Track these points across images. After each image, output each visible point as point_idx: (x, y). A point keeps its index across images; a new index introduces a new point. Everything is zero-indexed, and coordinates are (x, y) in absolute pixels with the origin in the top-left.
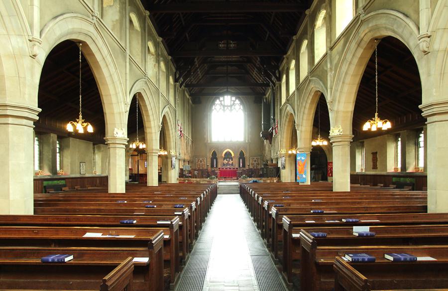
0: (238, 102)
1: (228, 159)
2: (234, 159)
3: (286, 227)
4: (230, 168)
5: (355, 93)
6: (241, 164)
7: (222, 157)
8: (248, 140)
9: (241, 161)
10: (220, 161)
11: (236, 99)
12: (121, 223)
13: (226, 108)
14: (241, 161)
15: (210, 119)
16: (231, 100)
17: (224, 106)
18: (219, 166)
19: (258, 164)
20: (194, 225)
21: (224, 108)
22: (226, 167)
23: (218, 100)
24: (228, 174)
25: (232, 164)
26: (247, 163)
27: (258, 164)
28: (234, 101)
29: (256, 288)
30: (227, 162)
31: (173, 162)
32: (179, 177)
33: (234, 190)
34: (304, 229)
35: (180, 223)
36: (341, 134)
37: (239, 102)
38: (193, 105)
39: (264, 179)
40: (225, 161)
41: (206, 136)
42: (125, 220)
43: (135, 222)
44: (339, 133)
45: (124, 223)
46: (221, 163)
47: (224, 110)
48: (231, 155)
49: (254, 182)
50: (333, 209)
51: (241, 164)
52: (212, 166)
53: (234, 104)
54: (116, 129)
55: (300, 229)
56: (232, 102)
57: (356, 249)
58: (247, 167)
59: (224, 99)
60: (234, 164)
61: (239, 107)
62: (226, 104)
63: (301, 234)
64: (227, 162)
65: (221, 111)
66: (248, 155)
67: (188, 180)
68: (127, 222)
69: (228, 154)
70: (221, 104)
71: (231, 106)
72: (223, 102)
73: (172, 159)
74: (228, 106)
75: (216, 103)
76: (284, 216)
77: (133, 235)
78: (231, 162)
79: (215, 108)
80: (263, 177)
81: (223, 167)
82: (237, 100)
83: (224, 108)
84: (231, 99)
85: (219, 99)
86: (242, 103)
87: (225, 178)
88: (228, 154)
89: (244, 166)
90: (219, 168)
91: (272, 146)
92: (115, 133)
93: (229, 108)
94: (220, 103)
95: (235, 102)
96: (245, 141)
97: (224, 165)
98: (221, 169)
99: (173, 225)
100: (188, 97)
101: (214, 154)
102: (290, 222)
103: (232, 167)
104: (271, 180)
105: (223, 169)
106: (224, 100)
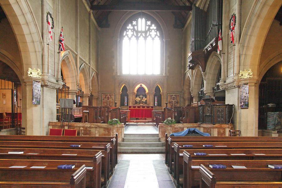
0: (153, 27)
1: (141, 96)
2: (148, 97)
3: (186, 160)
4: (143, 107)
5: (265, 36)
6: (156, 102)
7: (133, 93)
8: (166, 73)
9: (156, 99)
10: (131, 98)
11: (152, 23)
12: (71, 146)
13: (139, 34)
14: (156, 99)
15: (121, 48)
16: (146, 25)
17: (137, 32)
18: (130, 104)
19: (177, 103)
20: (99, 179)
21: (137, 34)
22: (139, 105)
23: (130, 25)
24: (141, 114)
25: (146, 103)
26: (164, 102)
27: (177, 103)
28: (150, 26)
29: (157, 185)
30: (139, 99)
31: (36, 91)
32: (58, 118)
33: (150, 145)
34: (186, 151)
35: (103, 155)
36: (252, 77)
37: (155, 28)
38: (99, 29)
39: (205, 125)
40: (138, 99)
41: (114, 67)
42: (74, 144)
43: (80, 146)
44: (249, 77)
45: (72, 146)
46: (131, 100)
47: (137, 37)
48: (145, 91)
49: (190, 132)
50: (225, 144)
51: (156, 102)
52: (122, 104)
53: (149, 29)
54: (30, 69)
55: (183, 151)
56: (147, 27)
57: (218, 161)
58: (164, 106)
59: (137, 23)
60: (148, 102)
61: (155, 33)
62: (139, 30)
63: (184, 154)
64: (139, 99)
65: (134, 38)
66: (165, 91)
67: (69, 126)
68: (74, 146)
69: (141, 89)
70: (134, 29)
71: (146, 32)
72: (136, 27)
73: (32, 85)
74: (142, 32)
75: (128, 28)
76: (175, 143)
77: (76, 154)
78: (144, 99)
79: (127, 35)
80: (204, 122)
81: (136, 105)
82: (153, 25)
83: (137, 34)
84: (146, 23)
85: (132, 23)
86: (159, 29)
87: (137, 119)
88: (141, 89)
89: (160, 104)
90: (130, 107)
91: (205, 75)
92: (29, 73)
93: (144, 34)
94: (132, 28)
95: (151, 28)
96: (163, 75)
97: (136, 102)
98: (132, 108)
99: (74, 180)
100: (88, 9)
101: (125, 89)
102: (190, 155)
103: (145, 105)
104: (221, 128)
105: (134, 107)
106: (137, 25)
